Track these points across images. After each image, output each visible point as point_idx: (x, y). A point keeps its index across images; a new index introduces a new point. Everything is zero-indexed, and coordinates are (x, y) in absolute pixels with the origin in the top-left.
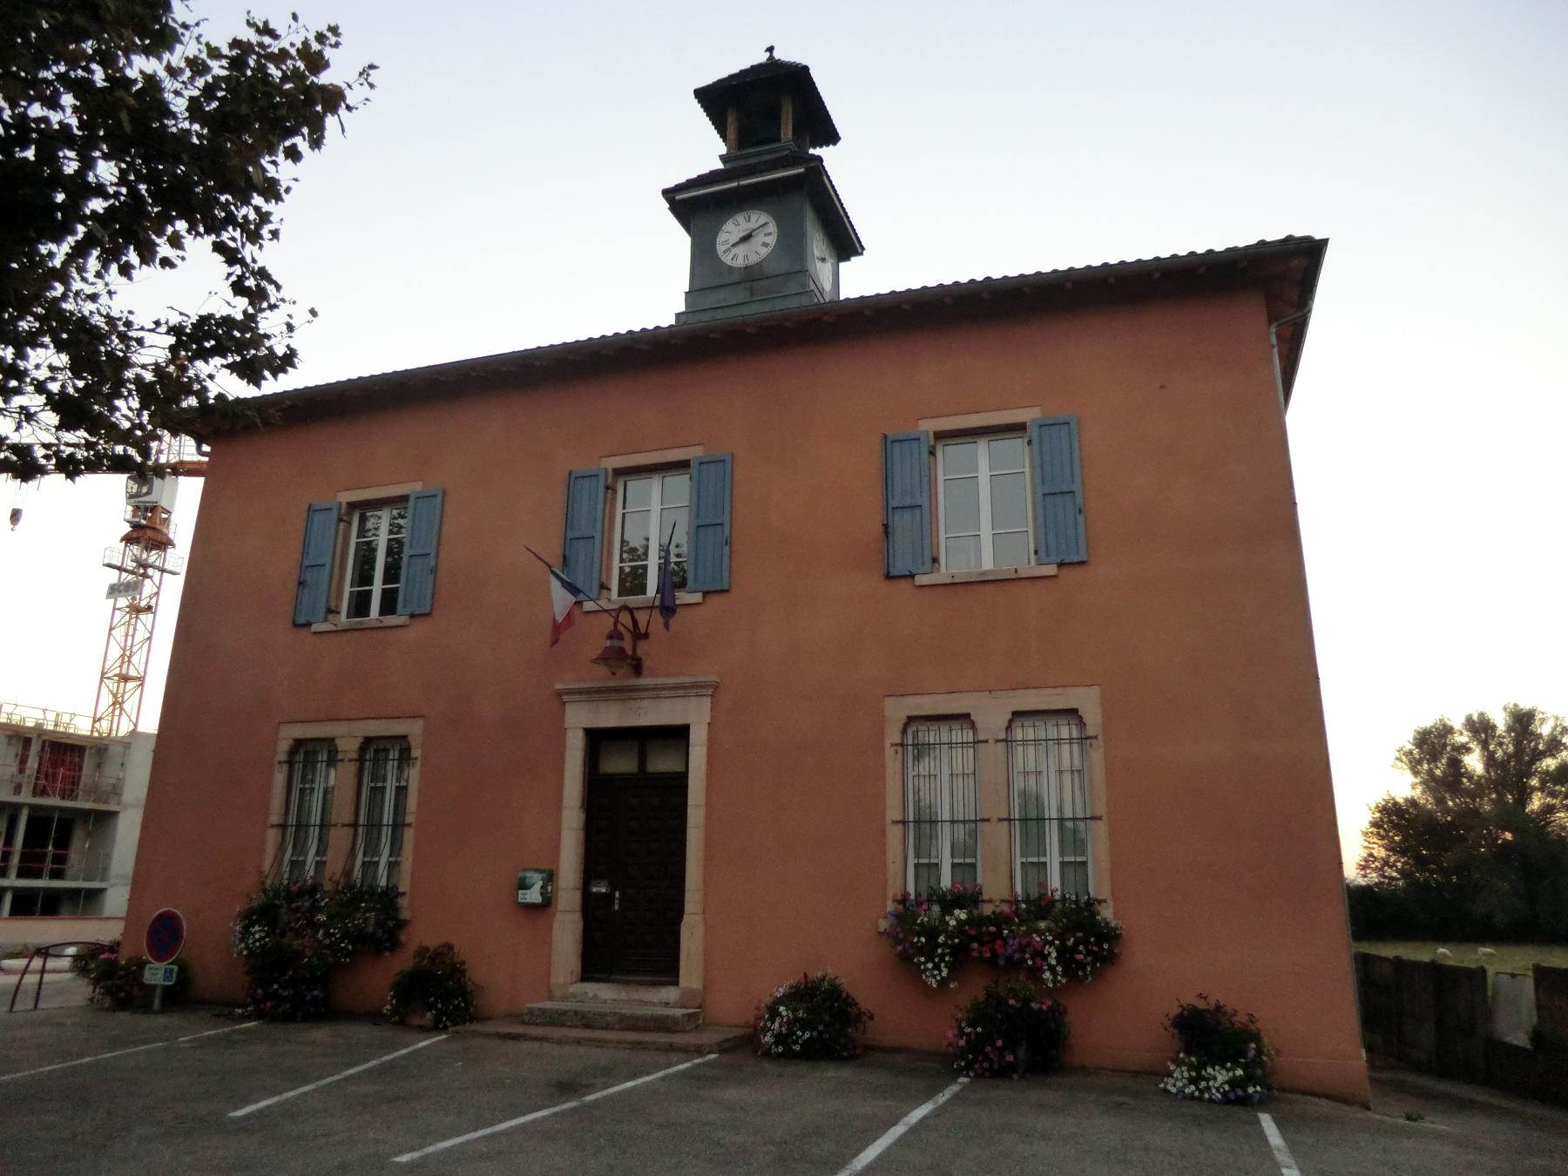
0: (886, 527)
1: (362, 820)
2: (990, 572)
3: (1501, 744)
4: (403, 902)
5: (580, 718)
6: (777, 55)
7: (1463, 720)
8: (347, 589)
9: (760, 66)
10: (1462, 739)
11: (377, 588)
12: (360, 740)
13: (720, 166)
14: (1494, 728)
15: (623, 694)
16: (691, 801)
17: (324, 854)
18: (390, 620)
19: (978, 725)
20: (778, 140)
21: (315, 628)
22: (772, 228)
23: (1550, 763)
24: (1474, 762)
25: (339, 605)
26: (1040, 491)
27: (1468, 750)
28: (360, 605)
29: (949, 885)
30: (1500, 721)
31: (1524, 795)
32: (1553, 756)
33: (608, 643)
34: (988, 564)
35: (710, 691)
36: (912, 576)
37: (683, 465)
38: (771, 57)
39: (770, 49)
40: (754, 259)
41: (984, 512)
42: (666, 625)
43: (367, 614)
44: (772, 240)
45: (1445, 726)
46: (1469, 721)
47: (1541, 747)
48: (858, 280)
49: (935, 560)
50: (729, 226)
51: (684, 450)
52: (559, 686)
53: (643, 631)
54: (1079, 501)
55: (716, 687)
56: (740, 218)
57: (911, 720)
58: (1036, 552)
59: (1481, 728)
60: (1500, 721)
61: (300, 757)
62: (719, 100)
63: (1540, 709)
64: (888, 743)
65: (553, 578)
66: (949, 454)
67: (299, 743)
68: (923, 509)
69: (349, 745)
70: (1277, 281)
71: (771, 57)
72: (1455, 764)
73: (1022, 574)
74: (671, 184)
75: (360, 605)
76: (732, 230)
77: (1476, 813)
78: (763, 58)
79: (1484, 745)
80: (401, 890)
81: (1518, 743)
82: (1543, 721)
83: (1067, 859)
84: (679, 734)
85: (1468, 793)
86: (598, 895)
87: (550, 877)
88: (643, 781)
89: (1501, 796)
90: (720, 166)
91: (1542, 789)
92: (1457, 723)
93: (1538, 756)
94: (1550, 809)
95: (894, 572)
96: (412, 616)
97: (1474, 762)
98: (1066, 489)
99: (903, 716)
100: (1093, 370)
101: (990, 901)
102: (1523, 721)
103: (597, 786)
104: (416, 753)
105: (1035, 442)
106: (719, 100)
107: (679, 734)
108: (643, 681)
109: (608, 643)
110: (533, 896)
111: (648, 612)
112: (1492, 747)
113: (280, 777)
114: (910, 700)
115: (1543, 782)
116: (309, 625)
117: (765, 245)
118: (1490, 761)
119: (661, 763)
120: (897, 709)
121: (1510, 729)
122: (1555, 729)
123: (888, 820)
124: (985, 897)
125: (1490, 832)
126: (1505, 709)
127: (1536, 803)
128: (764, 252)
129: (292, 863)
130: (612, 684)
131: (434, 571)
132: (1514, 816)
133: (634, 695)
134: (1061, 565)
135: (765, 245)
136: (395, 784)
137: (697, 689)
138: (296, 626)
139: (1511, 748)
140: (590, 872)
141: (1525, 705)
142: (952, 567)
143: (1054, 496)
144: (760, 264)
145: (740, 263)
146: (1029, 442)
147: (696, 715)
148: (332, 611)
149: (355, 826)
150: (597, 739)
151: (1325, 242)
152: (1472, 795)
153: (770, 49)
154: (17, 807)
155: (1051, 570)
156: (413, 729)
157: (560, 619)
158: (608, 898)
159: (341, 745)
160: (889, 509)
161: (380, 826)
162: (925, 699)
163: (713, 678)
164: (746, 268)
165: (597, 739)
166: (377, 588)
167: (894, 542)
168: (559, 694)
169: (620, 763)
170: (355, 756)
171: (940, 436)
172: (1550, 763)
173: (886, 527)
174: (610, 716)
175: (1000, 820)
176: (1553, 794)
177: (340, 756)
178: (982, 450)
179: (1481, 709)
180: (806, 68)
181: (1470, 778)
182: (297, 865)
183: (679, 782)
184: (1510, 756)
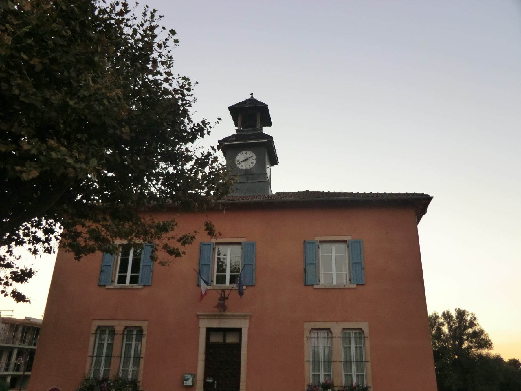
0: (305, 270)
1: (123, 355)
2: (335, 286)
3: (454, 323)
4: (140, 384)
5: (204, 324)
6: (255, 97)
7: (442, 313)
8: (117, 274)
9: (249, 100)
10: (442, 320)
11: (129, 274)
12: (124, 327)
13: (236, 133)
14: (452, 317)
15: (220, 317)
16: (242, 353)
17: (109, 366)
18: (135, 286)
19: (333, 332)
20: (255, 127)
21: (107, 287)
22: (255, 157)
23: (470, 331)
24: (445, 329)
25: (114, 280)
26: (351, 263)
27: (443, 325)
28: (122, 280)
29: (323, 381)
30: (454, 314)
31: (462, 342)
32: (471, 328)
33: (219, 302)
34: (334, 283)
35: (248, 318)
36: (313, 285)
37: (239, 244)
38: (252, 97)
39: (252, 94)
40: (248, 168)
41: (334, 267)
42: (241, 298)
43: (125, 283)
44: (254, 162)
45: (436, 316)
46: (444, 313)
47: (467, 324)
48: (283, 180)
49: (319, 281)
50: (240, 155)
51: (239, 239)
52: (198, 313)
53: (226, 297)
54: (363, 265)
55: (251, 316)
56: (244, 153)
57: (312, 329)
58: (350, 280)
59: (447, 316)
60: (454, 314)
61: (98, 332)
62: (235, 111)
63: (467, 310)
64: (305, 337)
65: (201, 280)
66: (323, 247)
67: (99, 327)
68: (315, 265)
69: (119, 328)
70: (417, 204)
71: (252, 97)
72: (439, 330)
73: (346, 287)
74: (221, 139)
75: (122, 280)
76: (241, 157)
77: (446, 348)
78: (249, 97)
79: (449, 324)
80: (139, 380)
81: (460, 322)
82: (468, 315)
83: (359, 374)
84: (239, 331)
85: (443, 340)
86: (209, 383)
87: (194, 376)
88: (224, 345)
89: (454, 342)
90: (236, 133)
91: (467, 340)
92: (440, 315)
93: (466, 328)
94: (470, 347)
95: (307, 284)
96: (144, 286)
97: (445, 329)
98: (358, 262)
99: (310, 328)
100: (366, 228)
101: (337, 386)
102: (461, 314)
103: (209, 346)
104: (145, 333)
105: (350, 247)
106: (235, 111)
107: (239, 331)
108: (227, 313)
109: (219, 302)
110: (189, 383)
111: (229, 291)
112: (451, 324)
113: (92, 339)
114: (312, 324)
115: (468, 338)
116: (105, 286)
117: (252, 163)
118: (450, 329)
119: (231, 339)
120: (308, 326)
121: (457, 318)
122: (471, 318)
123: (305, 360)
124: (335, 385)
125: (450, 355)
126: (455, 310)
127: (465, 345)
128: (252, 165)
129: (123, 370)
130: (220, 313)
131: (152, 271)
132: (458, 349)
133: (226, 317)
134: (357, 285)
135: (252, 163)
136: (356, 374)
137: (244, 317)
138: (99, 286)
139: (457, 325)
140: (207, 375)
141: (462, 309)
142: (323, 283)
143: (355, 264)
144: (250, 169)
145: (243, 168)
146: (348, 247)
147: (244, 325)
148: (113, 282)
149: (121, 357)
150: (209, 331)
151: (432, 198)
152: (445, 342)
153: (252, 94)
154: (13, 348)
155: (355, 286)
156: (144, 325)
157: (203, 293)
158: (213, 383)
159: (117, 329)
160: (305, 264)
161: (130, 357)
162: (318, 323)
163: (251, 314)
164: (246, 170)
165: (209, 331)
166: (129, 274)
167: (307, 272)
168: (198, 316)
169: (216, 339)
170: (122, 333)
171: (321, 242)
172: (470, 331)
173: (305, 270)
174: (215, 324)
175: (340, 361)
176: (471, 342)
177: (116, 333)
178: (333, 248)
179: (448, 310)
180: (267, 106)
181: (444, 335)
182: (97, 371)
183: (238, 346)
184: (457, 327)
